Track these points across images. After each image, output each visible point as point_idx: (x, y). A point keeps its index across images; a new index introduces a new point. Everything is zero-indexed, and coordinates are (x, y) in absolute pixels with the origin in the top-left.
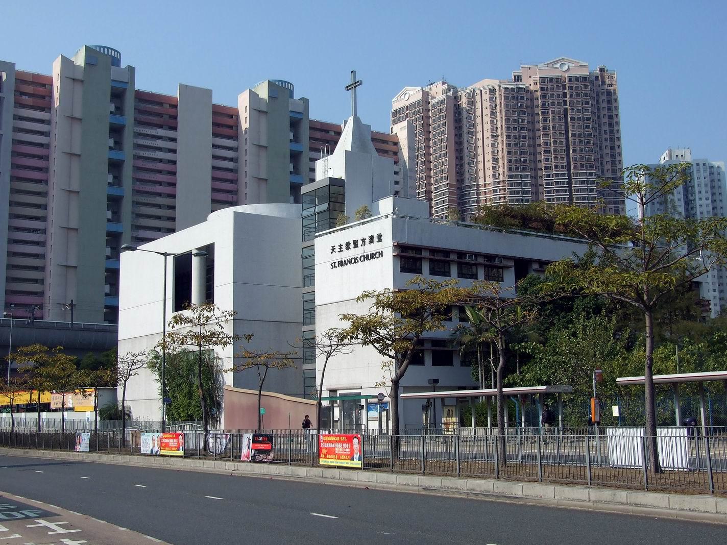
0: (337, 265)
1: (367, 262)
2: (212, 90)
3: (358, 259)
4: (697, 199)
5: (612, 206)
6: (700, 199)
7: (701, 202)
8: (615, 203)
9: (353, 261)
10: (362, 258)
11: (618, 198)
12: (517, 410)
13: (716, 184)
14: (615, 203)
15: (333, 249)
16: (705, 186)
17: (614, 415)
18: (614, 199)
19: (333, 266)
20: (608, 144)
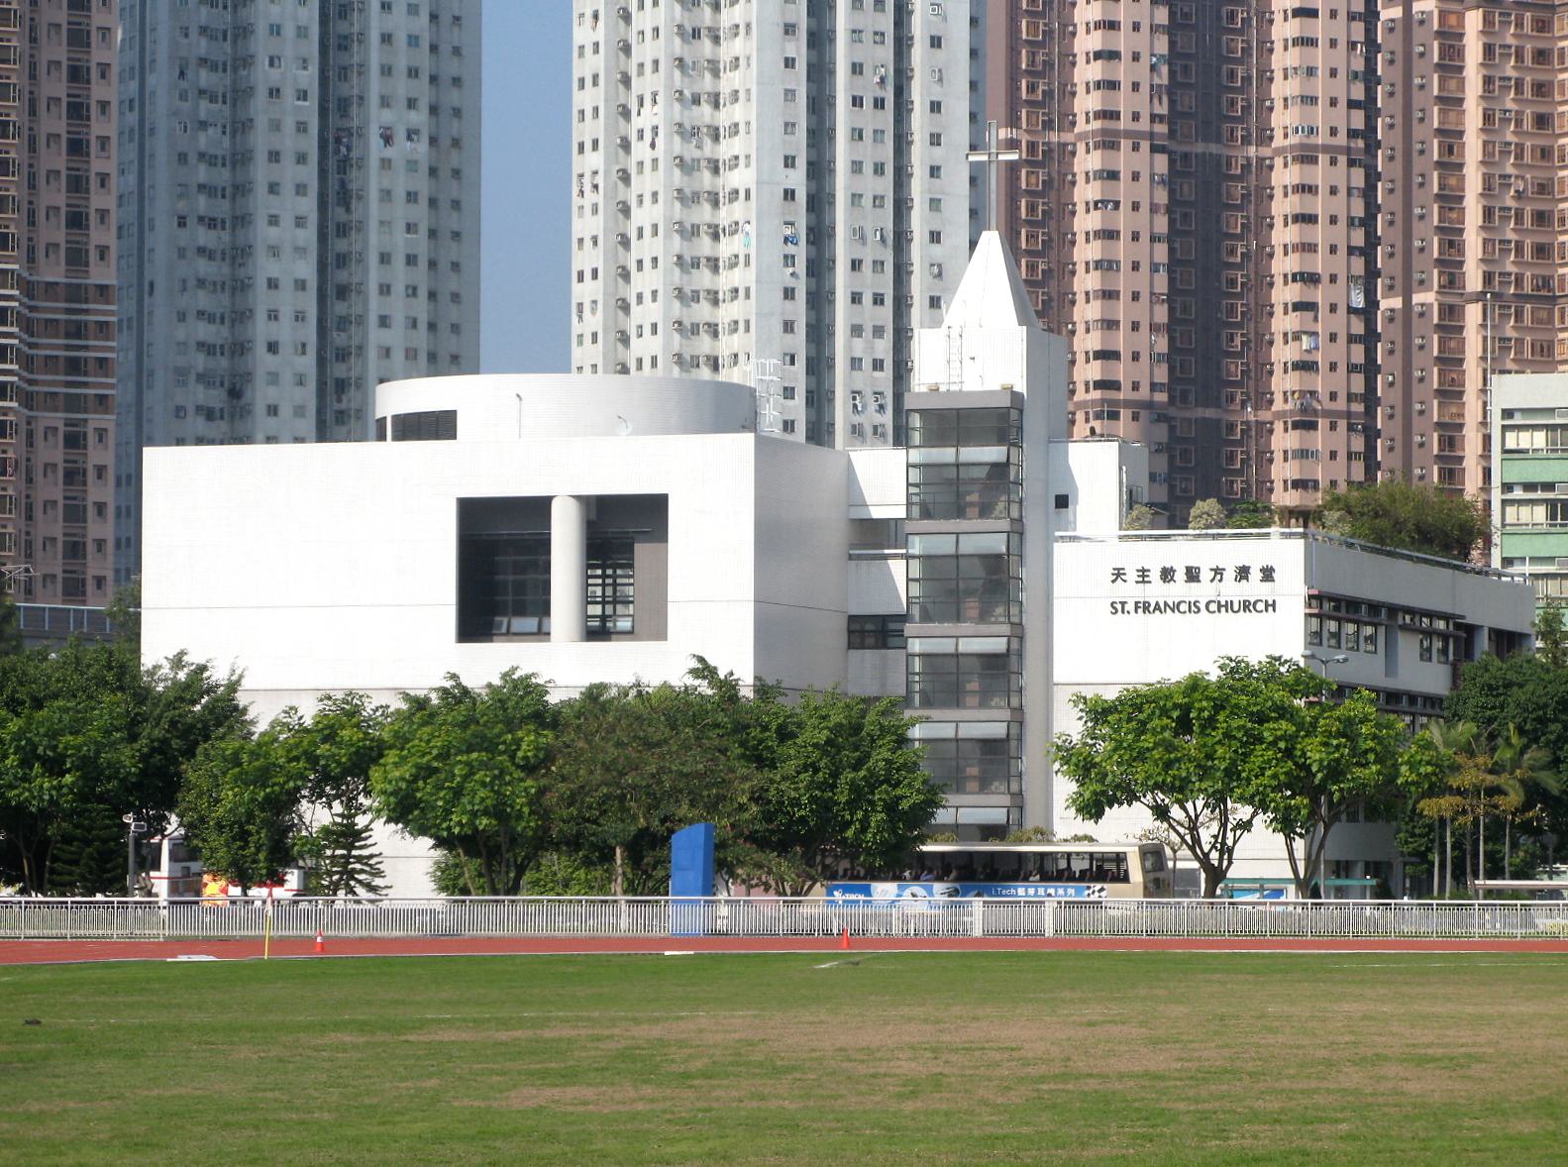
0: (1130, 607)
1: (1225, 616)
2: (665, 638)
3: (1202, 606)
4: (374, 100)
5: (57, 419)
6: (385, 102)
7: (387, 116)
8: (74, 403)
9: (1184, 607)
10: (1214, 607)
11: (85, 385)
12: (464, 1036)
13: (450, 37)
14: (74, 403)
15: (1118, 574)
16: (409, 44)
17: (157, 462)
18: (68, 384)
19: (1118, 608)
20: (58, 530)
